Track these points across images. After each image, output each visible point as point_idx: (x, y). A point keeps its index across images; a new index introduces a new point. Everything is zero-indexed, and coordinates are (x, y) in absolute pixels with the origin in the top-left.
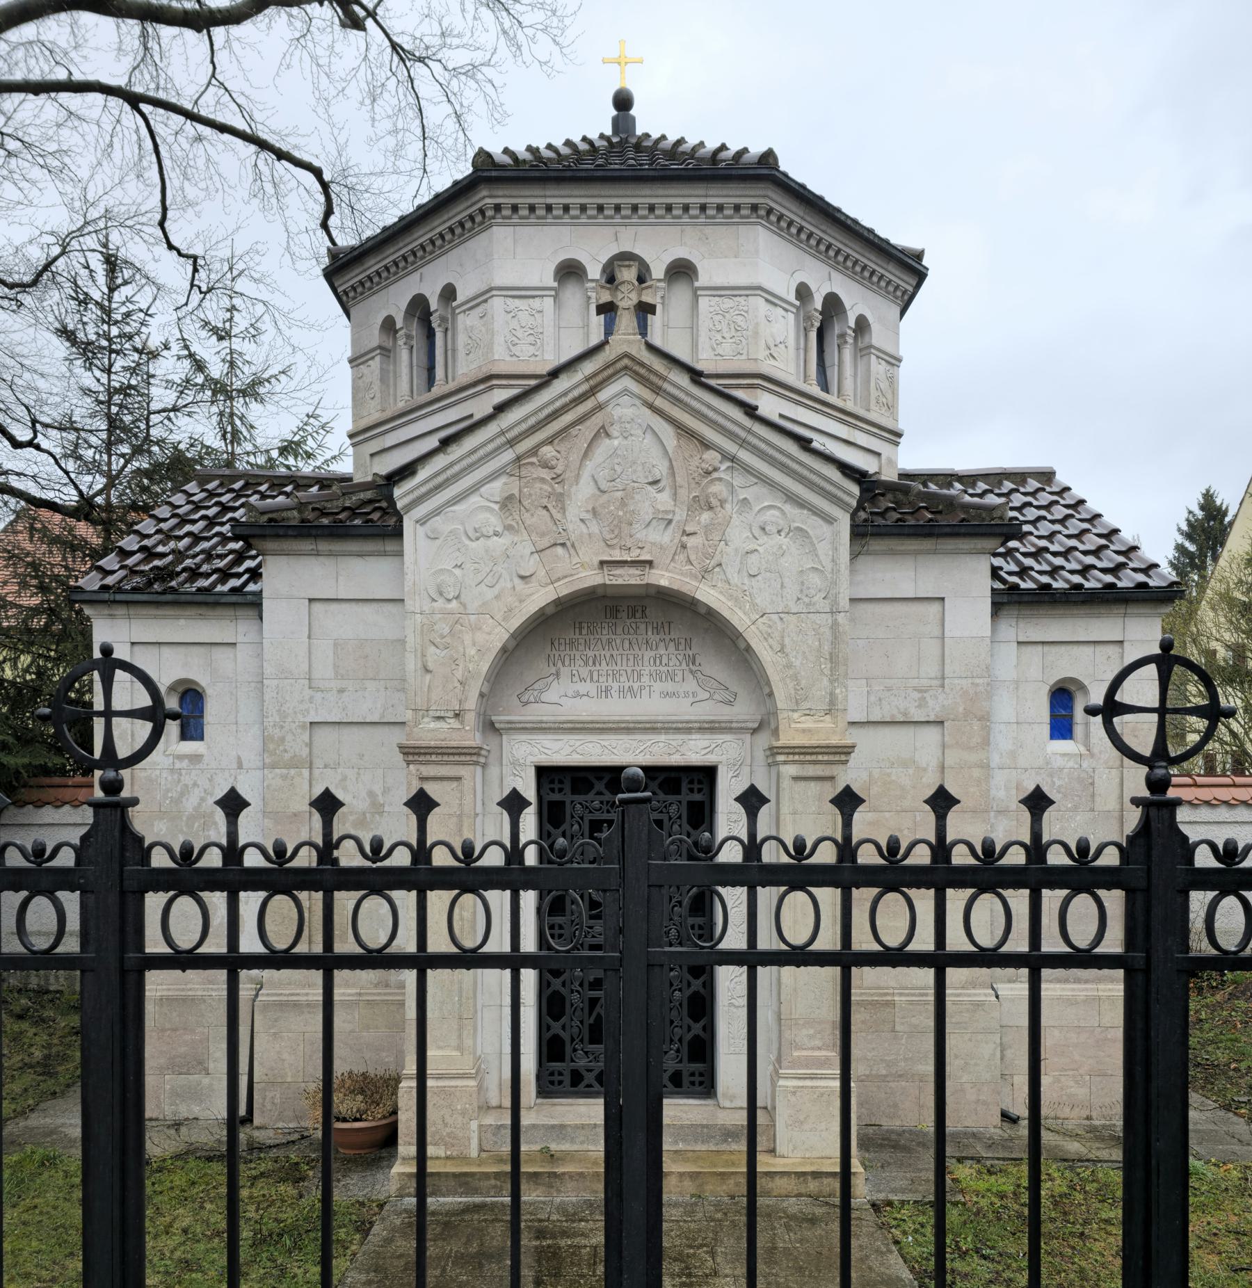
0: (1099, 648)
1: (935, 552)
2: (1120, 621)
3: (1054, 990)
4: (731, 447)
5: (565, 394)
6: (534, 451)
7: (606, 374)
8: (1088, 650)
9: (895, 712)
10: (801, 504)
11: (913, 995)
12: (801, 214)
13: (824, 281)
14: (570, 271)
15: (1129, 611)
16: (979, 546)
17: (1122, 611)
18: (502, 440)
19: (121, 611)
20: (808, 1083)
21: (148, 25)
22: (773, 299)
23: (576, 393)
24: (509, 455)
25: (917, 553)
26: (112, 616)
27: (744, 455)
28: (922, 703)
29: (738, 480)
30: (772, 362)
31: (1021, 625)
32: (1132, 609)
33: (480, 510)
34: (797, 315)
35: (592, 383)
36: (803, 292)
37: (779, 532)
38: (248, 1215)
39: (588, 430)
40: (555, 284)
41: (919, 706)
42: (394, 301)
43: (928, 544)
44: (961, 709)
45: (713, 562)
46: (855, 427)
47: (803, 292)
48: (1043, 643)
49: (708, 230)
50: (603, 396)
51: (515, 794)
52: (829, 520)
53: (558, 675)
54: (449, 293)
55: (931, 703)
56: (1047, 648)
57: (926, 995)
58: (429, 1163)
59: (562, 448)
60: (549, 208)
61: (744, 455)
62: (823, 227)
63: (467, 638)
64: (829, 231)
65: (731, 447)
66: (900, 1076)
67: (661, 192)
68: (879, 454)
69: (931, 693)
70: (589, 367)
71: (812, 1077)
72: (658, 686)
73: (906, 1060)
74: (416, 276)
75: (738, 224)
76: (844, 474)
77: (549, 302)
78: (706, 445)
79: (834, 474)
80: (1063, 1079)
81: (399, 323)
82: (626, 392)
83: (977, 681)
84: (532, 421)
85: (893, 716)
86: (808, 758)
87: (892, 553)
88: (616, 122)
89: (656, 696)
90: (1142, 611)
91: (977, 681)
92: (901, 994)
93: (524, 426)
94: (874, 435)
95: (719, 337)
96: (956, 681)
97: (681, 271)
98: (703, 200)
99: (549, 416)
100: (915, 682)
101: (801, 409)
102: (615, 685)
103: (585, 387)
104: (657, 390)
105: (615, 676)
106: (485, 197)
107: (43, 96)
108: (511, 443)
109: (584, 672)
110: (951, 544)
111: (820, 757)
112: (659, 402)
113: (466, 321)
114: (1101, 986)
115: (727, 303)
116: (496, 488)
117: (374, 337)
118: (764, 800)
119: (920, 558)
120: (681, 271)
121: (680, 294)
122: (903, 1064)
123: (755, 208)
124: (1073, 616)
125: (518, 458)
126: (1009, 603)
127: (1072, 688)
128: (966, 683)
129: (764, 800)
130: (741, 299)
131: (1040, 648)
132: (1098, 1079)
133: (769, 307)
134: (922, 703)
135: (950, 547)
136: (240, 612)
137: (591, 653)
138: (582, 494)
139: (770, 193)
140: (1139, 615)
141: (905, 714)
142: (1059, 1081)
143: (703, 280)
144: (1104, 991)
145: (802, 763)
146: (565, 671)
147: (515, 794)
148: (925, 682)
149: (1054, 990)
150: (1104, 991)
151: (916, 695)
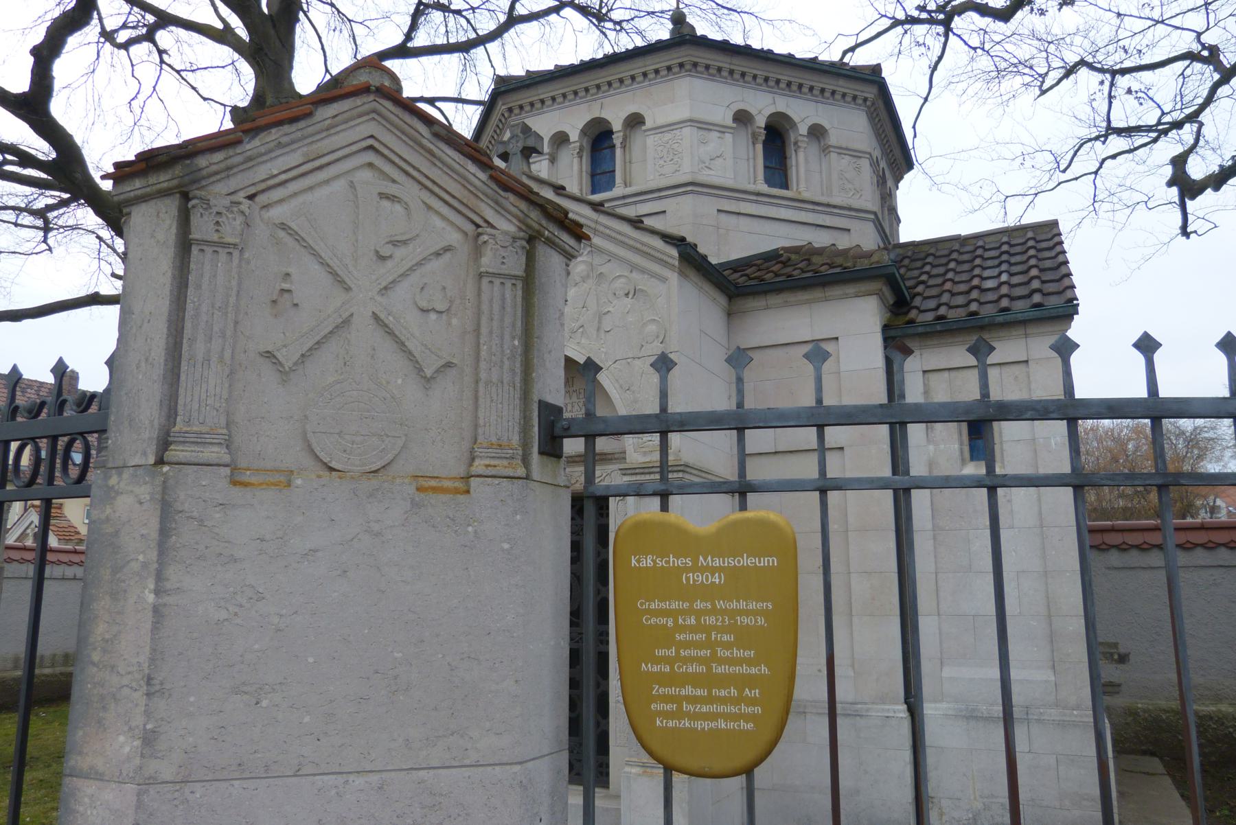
0: (1006, 369)
2: (1022, 342)
5: (619, 233)
10: (643, 271)
13: (763, 105)
14: (742, 118)
15: (1029, 331)
21: (473, 36)
37: (627, 295)
43: (818, 293)
52: (663, 280)
56: (953, 374)
58: (31, 573)
79: (658, 243)
87: (787, 304)
90: (1050, 329)
95: (662, 162)
98: (643, 70)
101: (742, 204)
107: (1127, 76)
110: (837, 291)
115: (668, 136)
123: (681, 65)
130: (677, 132)
131: (946, 374)
133: (701, 132)
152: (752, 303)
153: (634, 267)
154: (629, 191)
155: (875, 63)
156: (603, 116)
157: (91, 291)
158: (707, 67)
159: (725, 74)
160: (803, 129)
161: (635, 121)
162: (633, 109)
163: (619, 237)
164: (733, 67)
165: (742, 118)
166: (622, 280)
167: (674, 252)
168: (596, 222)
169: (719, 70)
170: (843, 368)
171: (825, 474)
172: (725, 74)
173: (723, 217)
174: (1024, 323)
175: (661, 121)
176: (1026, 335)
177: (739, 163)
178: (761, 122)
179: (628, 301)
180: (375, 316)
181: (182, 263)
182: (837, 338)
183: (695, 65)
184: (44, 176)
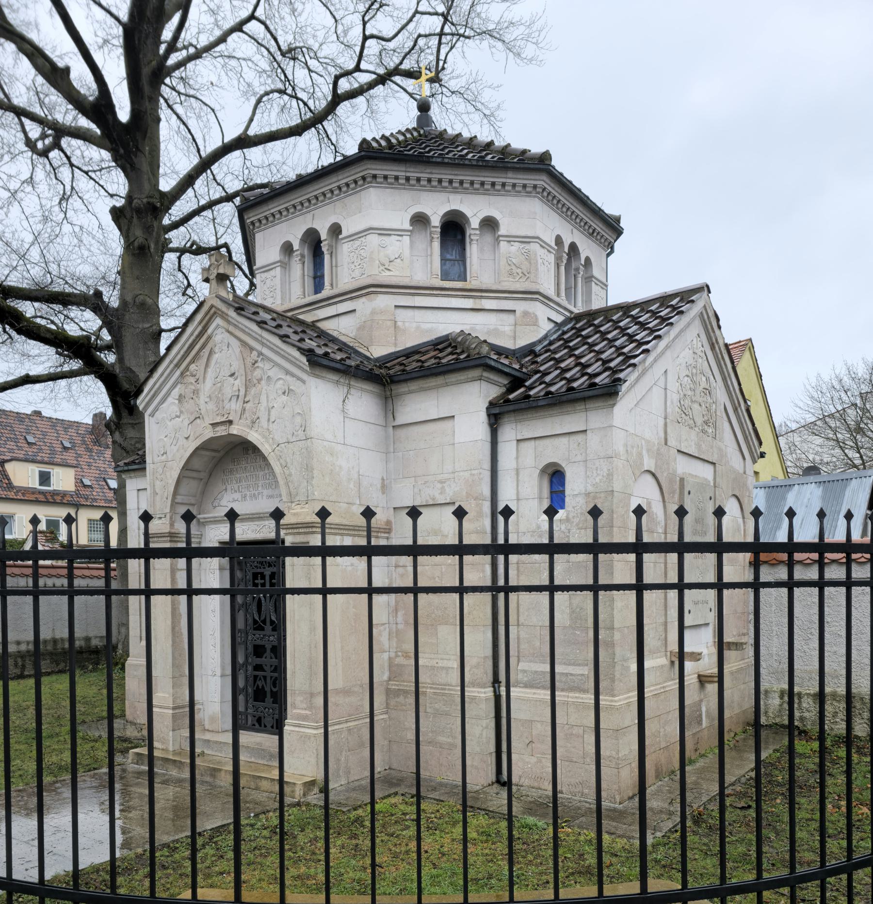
1: (447, 385)
2: (583, 415)
3: (539, 694)
6: (187, 368)
7: (207, 318)
8: (564, 440)
9: (428, 498)
10: (293, 375)
11: (438, 689)
12: (404, 169)
14: (420, 220)
16: (470, 376)
17: (583, 407)
18: (172, 366)
20: (297, 729)
22: (544, 245)
23: (196, 333)
24: (178, 373)
25: (437, 387)
28: (442, 491)
30: (388, 273)
31: (519, 426)
32: (590, 405)
33: (171, 406)
35: (202, 325)
36: (559, 240)
39: (206, 352)
40: (411, 228)
41: (441, 493)
43: (440, 380)
44: (464, 493)
45: (256, 417)
46: (482, 297)
47: (559, 240)
48: (535, 438)
49: (346, 200)
50: (209, 331)
53: (226, 489)
54: (336, 230)
55: (447, 490)
57: (455, 691)
59: (198, 364)
60: (408, 179)
62: (428, 171)
63: (168, 474)
64: (434, 171)
66: (429, 742)
67: (316, 187)
68: (514, 311)
69: (448, 483)
70: (199, 317)
71: (299, 726)
73: (432, 732)
75: (360, 191)
76: (301, 353)
78: (252, 349)
80: (544, 760)
81: (296, 246)
82: (218, 326)
83: (473, 472)
84: (182, 353)
85: (427, 501)
86: (295, 531)
88: (419, 119)
89: (265, 497)
90: (600, 404)
91: (473, 472)
92: (431, 688)
93: (179, 356)
94: (506, 298)
96: (462, 474)
97: (490, 224)
99: (189, 348)
100: (440, 477)
101: (417, 298)
102: (248, 493)
103: (200, 328)
105: (248, 487)
108: (178, 366)
109: (236, 486)
110: (453, 378)
111: (301, 530)
112: (231, 329)
114: (571, 695)
115: (357, 243)
116: (176, 392)
118: (645, 512)
119: (440, 390)
122: (430, 734)
124: (551, 416)
125: (182, 374)
126: (509, 412)
128: (467, 474)
129: (645, 512)
130: (362, 239)
131: (533, 442)
132: (567, 763)
134: (442, 491)
135: (453, 380)
137: (238, 476)
138: (207, 387)
139: (369, 166)
140: (596, 409)
141: (433, 499)
142: (540, 762)
144: (572, 698)
145: (354, 535)
146: (229, 487)
148: (446, 476)
149: (539, 694)
150: (572, 698)
151: (439, 486)
152: (403, 388)
153: (288, 372)
154: (336, 291)
155: (544, 150)
156: (314, 226)
157: (23, 373)
158: (386, 177)
159: (402, 181)
160: (475, 223)
161: (336, 230)
162: (333, 219)
163: (275, 348)
164: (408, 174)
165: (420, 220)
166: (281, 382)
167: (304, 359)
168: (261, 336)
169: (397, 178)
170: (456, 441)
171: (597, 540)
172: (402, 181)
173: (399, 311)
174: (584, 399)
175: (352, 231)
176: (586, 410)
177: (422, 261)
178: (436, 221)
179: (285, 398)
180: (549, 319)
181: (460, 164)
182: (453, 417)
183: (375, 177)
184: (93, 127)
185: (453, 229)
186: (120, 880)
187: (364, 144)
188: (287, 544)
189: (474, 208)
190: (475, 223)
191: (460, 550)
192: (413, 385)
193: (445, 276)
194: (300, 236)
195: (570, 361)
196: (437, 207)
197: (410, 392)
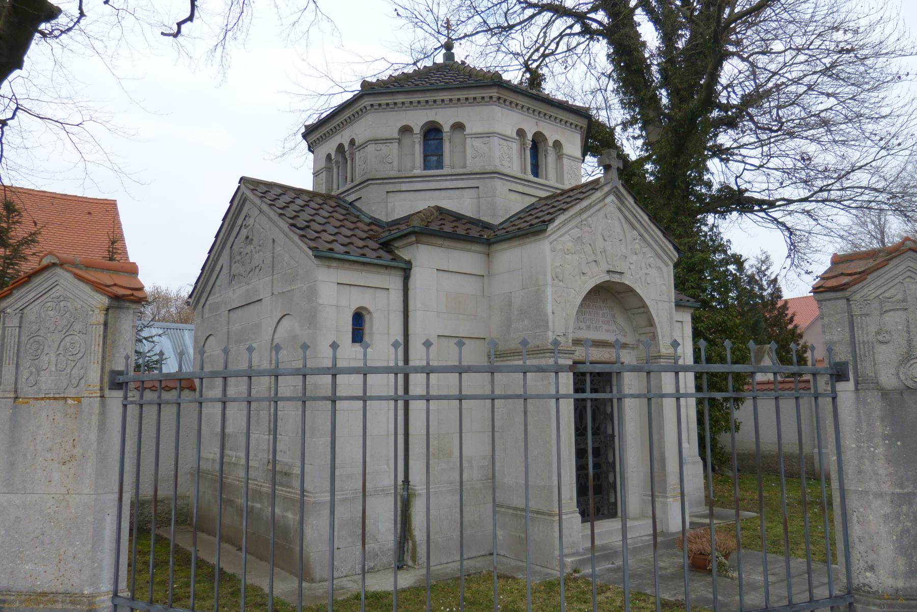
4: (642, 231)
19: (334, 264)
22: (504, 137)
26: (329, 267)
27: (645, 235)
29: (643, 244)
34: (519, 143)
36: (521, 133)
38: (853, 488)
42: (330, 147)
47: (521, 133)
51: (397, 341)
52: (667, 265)
54: (352, 142)
61: (645, 235)
65: (642, 231)
72: (605, 327)
74: (340, 135)
77: (396, 145)
97: (458, 127)
101: (441, 183)
104: (623, 203)
106: (367, 102)
113: (358, 155)
117: (323, 163)
118: (308, 347)
120: (458, 127)
121: (457, 137)
127: (364, 313)
129: (308, 347)
136: (393, 272)
143: (468, 130)
147: (397, 341)
161: (352, 142)
177: (512, 159)
178: (417, 130)
185: (432, 132)
186: (805, 567)
187: (365, 84)
188: (805, 355)
189: (445, 118)
190: (446, 128)
191: (461, 370)
192: (505, 245)
193: (426, 167)
194: (335, 149)
195: (318, 218)
196: (418, 119)
197: (501, 250)
